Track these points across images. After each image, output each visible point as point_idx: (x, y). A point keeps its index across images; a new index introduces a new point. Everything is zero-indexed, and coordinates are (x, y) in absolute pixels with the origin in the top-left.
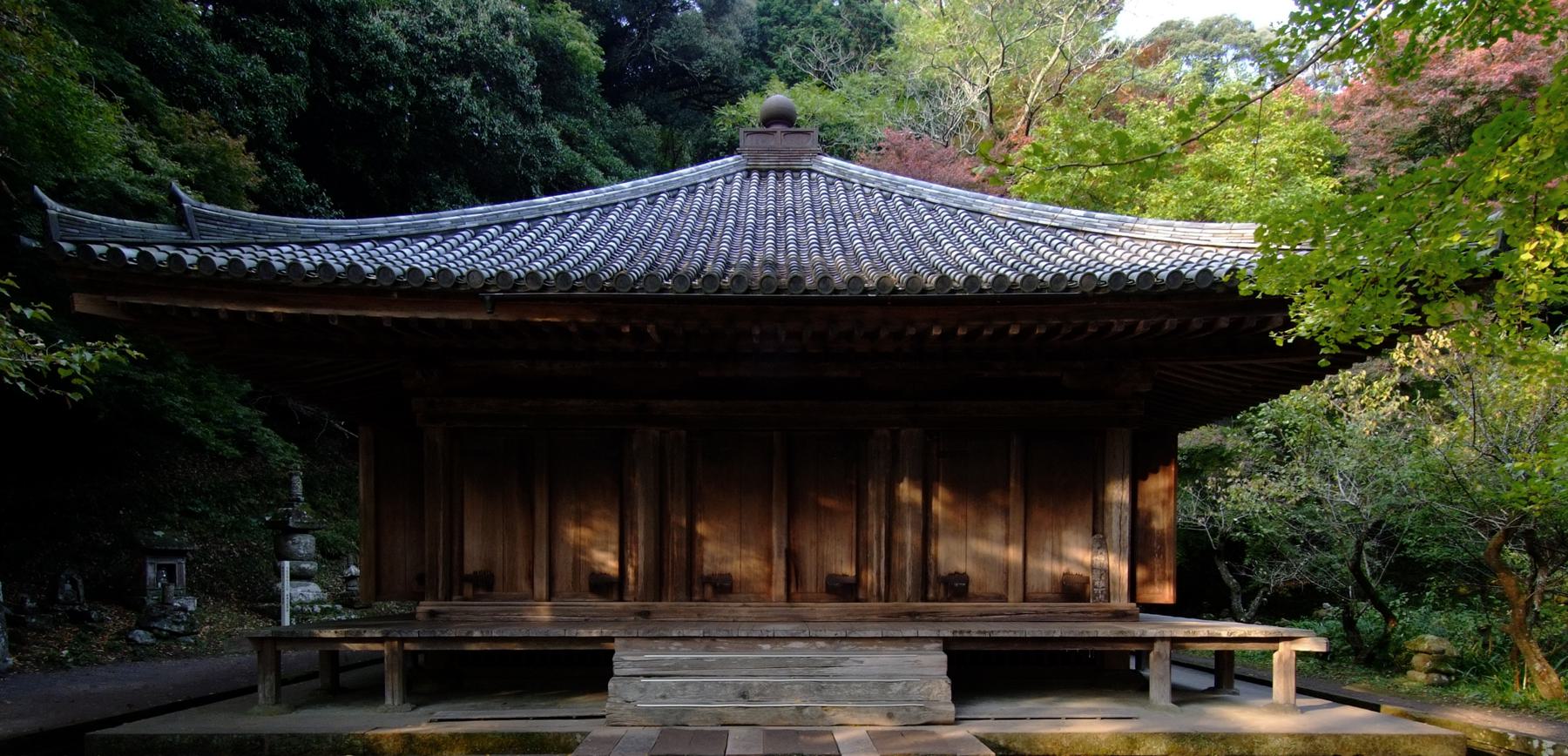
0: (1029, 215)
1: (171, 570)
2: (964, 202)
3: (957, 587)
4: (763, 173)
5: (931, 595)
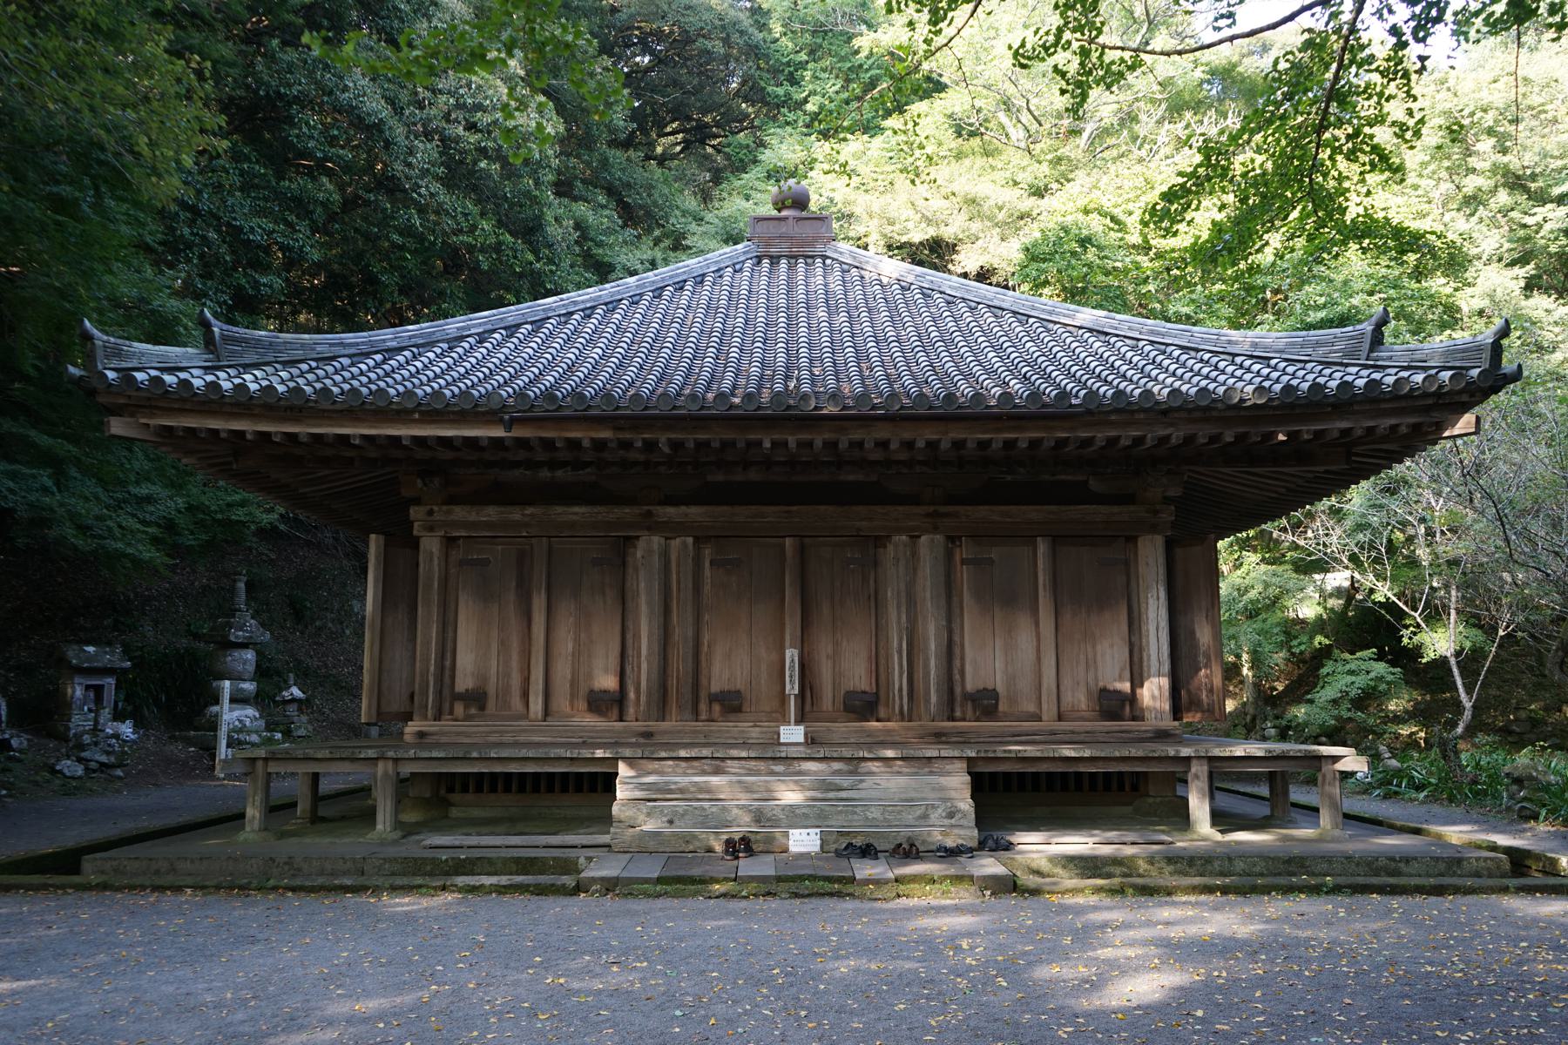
0: (1050, 313)
1: (99, 689)
2: (985, 297)
3: (986, 704)
4: (775, 261)
5: (958, 714)
